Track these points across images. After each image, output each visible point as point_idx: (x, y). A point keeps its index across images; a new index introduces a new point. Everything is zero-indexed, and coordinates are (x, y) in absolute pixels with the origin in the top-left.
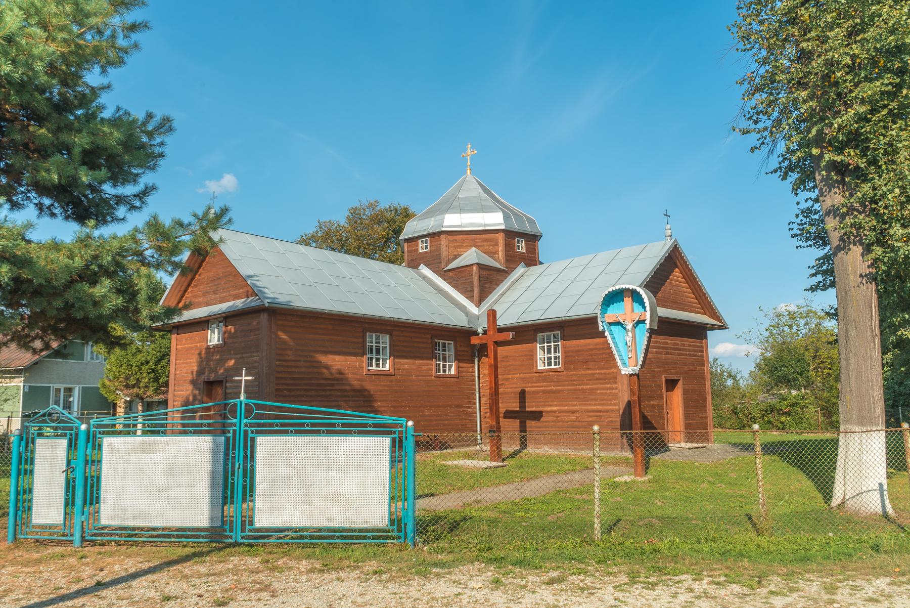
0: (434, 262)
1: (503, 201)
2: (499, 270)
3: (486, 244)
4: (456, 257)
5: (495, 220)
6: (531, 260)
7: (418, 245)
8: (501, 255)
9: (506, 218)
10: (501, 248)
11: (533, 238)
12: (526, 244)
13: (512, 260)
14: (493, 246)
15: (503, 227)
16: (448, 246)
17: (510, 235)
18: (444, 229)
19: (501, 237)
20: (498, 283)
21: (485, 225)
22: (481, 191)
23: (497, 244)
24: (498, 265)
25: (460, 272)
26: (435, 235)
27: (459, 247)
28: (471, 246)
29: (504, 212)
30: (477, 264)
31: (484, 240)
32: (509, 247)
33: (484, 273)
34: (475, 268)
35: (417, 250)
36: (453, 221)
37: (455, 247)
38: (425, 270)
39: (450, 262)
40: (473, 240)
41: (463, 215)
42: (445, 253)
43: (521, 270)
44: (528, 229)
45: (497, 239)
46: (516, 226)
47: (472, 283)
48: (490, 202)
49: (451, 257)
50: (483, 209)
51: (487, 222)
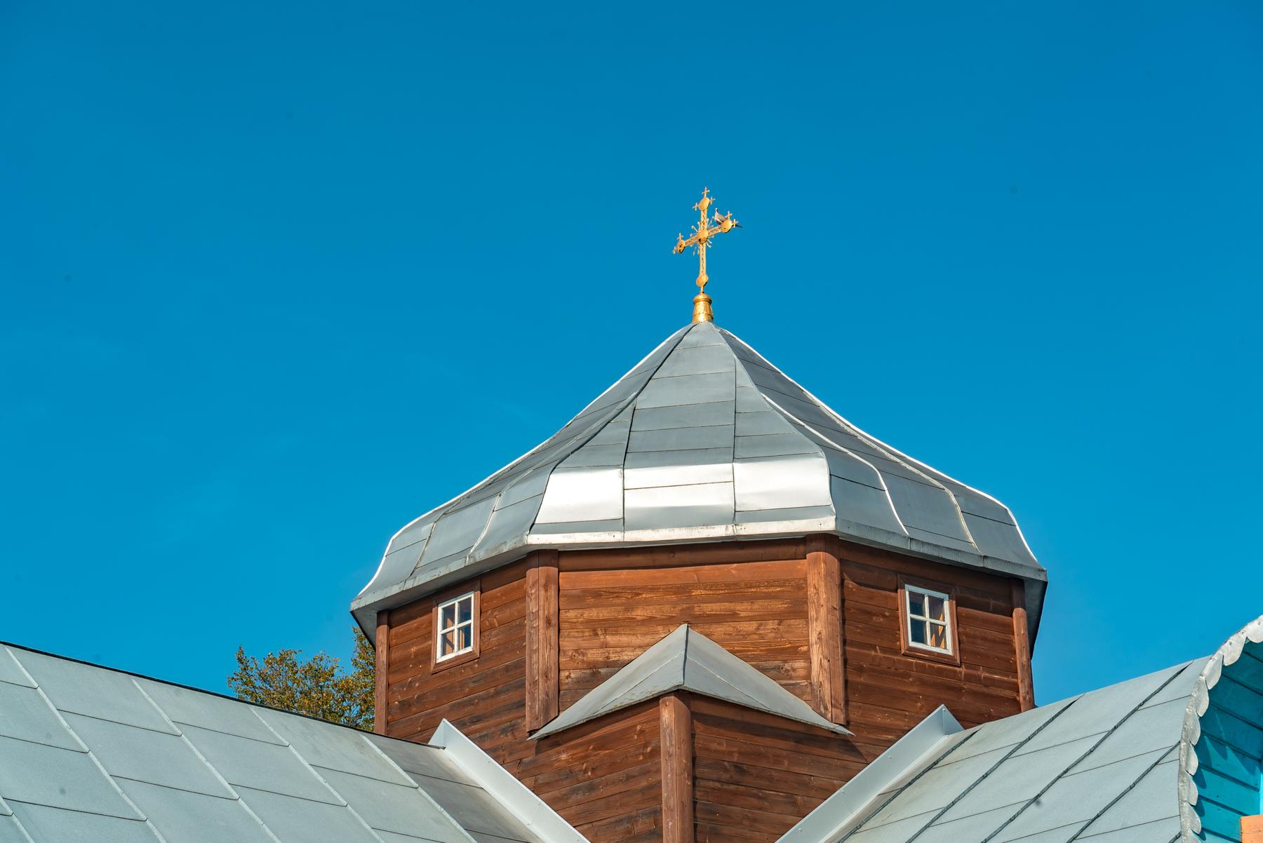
0: (489, 702)
1: (854, 429)
2: (805, 735)
3: (743, 608)
4: (594, 677)
5: (789, 489)
6: (983, 691)
7: (429, 634)
8: (820, 661)
9: (844, 480)
10: (819, 629)
11: (996, 593)
12: (959, 620)
13: (883, 694)
14: (781, 617)
15: (827, 524)
16: (557, 624)
17: (865, 564)
18: (536, 539)
19: (818, 574)
20: (802, 799)
21: (736, 516)
22: (745, 379)
23: (799, 610)
24: (804, 712)
25: (602, 744)
26: (500, 573)
27: (611, 626)
28: (670, 622)
29: (830, 453)
30: (680, 693)
31: (735, 592)
32: (861, 629)
33: (719, 743)
34: (668, 714)
35: (428, 654)
36: (580, 500)
37: (595, 627)
38: (457, 751)
39: (561, 698)
40: (682, 590)
41: (636, 476)
42: (540, 656)
43: (929, 738)
44: (967, 542)
45: (801, 586)
46: (895, 524)
47: (653, 792)
48: (779, 418)
49: (572, 675)
50: (738, 447)
51: (749, 503)
